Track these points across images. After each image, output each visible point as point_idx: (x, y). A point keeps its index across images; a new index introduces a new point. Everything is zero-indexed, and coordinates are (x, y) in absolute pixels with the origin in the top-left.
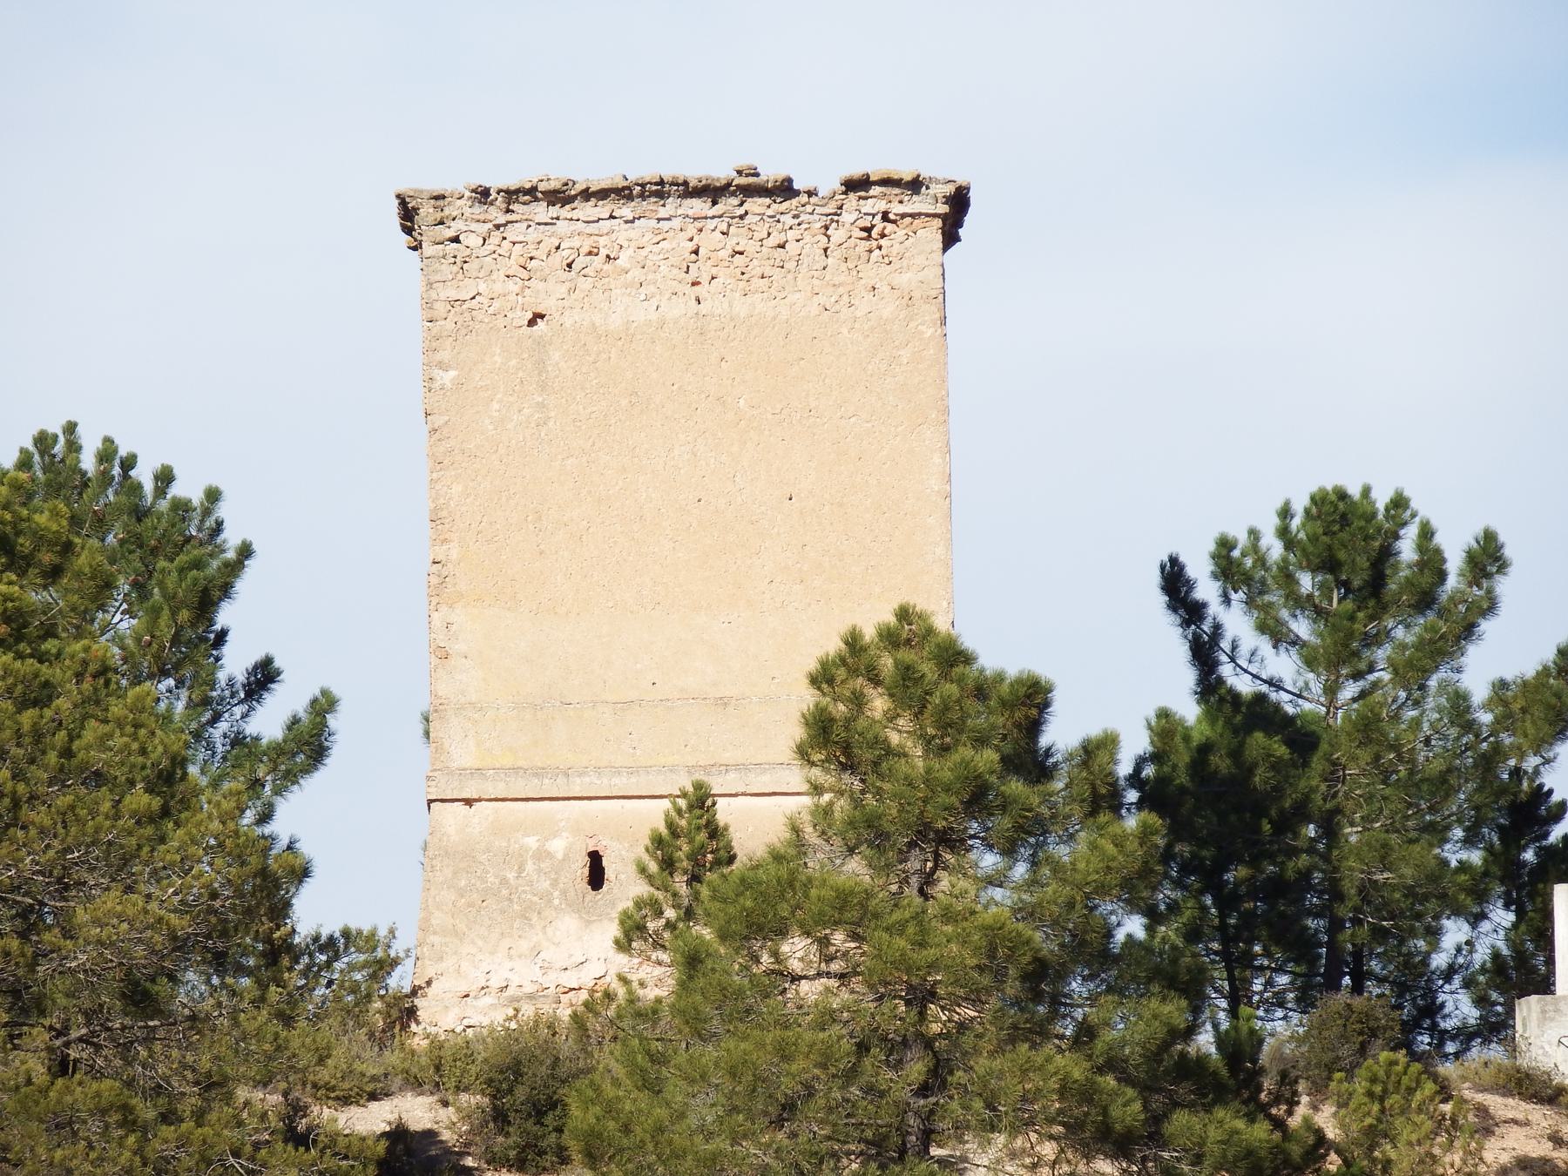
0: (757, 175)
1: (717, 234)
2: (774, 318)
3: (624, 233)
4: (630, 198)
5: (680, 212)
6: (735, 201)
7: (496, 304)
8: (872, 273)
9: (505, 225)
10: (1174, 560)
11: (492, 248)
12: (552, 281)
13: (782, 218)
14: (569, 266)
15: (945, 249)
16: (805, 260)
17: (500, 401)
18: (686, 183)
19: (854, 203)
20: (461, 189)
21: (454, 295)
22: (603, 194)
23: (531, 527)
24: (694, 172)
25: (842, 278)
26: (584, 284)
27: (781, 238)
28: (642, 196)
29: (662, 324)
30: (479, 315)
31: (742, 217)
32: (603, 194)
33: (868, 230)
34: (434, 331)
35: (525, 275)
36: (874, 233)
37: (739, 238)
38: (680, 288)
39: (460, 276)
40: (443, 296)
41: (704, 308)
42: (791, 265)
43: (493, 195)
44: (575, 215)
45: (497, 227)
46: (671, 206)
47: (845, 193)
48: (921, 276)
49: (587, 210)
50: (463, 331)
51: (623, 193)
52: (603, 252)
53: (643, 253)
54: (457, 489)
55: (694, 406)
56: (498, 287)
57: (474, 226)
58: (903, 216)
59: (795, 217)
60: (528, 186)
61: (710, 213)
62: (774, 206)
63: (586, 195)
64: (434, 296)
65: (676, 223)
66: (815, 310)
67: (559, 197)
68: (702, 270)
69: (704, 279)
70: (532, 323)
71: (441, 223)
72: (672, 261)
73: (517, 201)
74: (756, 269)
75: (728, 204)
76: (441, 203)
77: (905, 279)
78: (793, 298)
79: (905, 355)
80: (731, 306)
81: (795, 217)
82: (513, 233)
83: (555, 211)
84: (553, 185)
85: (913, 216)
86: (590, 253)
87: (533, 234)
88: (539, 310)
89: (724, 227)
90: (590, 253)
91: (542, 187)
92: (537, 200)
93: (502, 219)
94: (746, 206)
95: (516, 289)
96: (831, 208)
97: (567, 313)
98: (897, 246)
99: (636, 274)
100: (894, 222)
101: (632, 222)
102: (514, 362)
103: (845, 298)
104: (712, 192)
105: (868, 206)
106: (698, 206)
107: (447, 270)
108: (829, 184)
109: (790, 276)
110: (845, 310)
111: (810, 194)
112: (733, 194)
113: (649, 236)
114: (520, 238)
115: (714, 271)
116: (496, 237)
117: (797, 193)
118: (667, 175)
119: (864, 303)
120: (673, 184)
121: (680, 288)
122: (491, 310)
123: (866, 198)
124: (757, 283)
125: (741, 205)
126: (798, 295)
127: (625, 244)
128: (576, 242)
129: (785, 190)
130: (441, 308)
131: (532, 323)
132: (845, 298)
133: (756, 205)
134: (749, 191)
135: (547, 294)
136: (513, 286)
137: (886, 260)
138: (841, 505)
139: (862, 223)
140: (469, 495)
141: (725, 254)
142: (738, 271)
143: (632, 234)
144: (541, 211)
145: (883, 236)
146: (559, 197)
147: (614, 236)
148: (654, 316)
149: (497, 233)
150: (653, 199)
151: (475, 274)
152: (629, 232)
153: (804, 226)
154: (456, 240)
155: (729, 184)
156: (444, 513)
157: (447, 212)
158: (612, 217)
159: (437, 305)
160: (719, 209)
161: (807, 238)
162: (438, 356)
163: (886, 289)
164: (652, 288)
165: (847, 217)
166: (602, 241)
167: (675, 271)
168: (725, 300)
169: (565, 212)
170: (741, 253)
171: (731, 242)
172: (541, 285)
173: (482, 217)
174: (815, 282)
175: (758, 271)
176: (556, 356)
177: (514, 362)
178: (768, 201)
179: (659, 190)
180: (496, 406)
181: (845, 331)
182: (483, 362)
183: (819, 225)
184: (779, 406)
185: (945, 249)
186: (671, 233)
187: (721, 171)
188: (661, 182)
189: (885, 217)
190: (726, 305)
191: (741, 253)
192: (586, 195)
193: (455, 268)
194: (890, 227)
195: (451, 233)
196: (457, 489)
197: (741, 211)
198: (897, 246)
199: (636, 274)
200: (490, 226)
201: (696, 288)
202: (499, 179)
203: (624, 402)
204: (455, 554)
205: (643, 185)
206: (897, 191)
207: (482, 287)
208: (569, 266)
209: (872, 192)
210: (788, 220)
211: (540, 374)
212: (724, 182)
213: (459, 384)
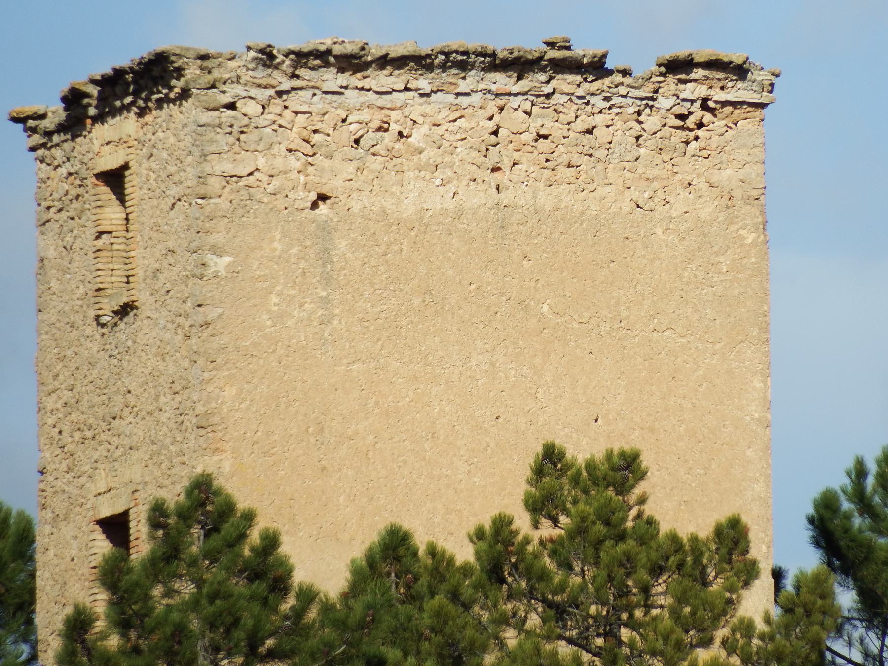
0: (568, 48)
1: (520, 114)
2: (583, 213)
3: (417, 107)
4: (430, 68)
5: (481, 86)
6: (543, 77)
7: (276, 182)
8: (688, 168)
9: (287, 92)
10: (735, 523)
11: (271, 117)
12: (338, 156)
13: (593, 100)
14: (357, 141)
15: (126, 167)
16: (617, 149)
17: (279, 295)
18: (494, 55)
19: (673, 87)
20: (240, 49)
21: (229, 168)
22: (400, 62)
23: (312, 440)
24: (502, 44)
25: (656, 172)
26: (375, 164)
27: (590, 122)
28: (444, 67)
29: (460, 213)
30: (258, 194)
31: (548, 96)
32: (400, 62)
33: (682, 117)
34: (208, 209)
35: (308, 150)
36: (691, 122)
37: (543, 120)
38: (480, 174)
39: (236, 148)
40: (218, 169)
41: (506, 197)
42: (601, 154)
43: (280, 58)
44: (366, 83)
45: (280, 94)
46: (471, 81)
47: (662, 75)
48: (742, 174)
49: (380, 79)
50: (240, 212)
51: (421, 62)
52: (394, 128)
53: (440, 130)
54: (230, 392)
55: (494, 309)
56: (279, 163)
57: (254, 92)
58: (724, 104)
59: (607, 99)
60: (322, 48)
61: (515, 89)
62: (586, 86)
63: (384, 62)
64: (208, 170)
65: (476, 99)
66: (627, 206)
67: (352, 63)
68: (503, 154)
69: (506, 164)
70: (314, 205)
71: (213, 87)
72: (470, 141)
73: (306, 66)
74: (562, 154)
75: (535, 80)
76: (207, 63)
77: (726, 176)
78: (601, 192)
79: (725, 261)
80: (535, 197)
81: (607, 99)
82: (295, 101)
83: (344, 79)
84: (350, 49)
85: (734, 104)
86: (380, 129)
87: (319, 103)
88: (324, 191)
89: (527, 106)
90: (380, 129)
91: (337, 50)
92: (327, 64)
93: (286, 85)
94: (554, 83)
95: (298, 165)
96: (645, 92)
97: (355, 195)
98: (716, 138)
99: (431, 154)
100: (712, 111)
101: (428, 95)
102: (295, 250)
103: (660, 194)
104: (520, 65)
105: (692, 91)
106: (502, 81)
107: (223, 141)
108: (645, 64)
109: (600, 166)
110: (659, 208)
111: (625, 73)
112: (543, 69)
113: (445, 112)
114: (304, 108)
115: (516, 156)
116: (276, 106)
117: (610, 73)
118: (473, 44)
119: (681, 200)
120: (483, 54)
121: (480, 174)
122: (270, 189)
123: (685, 82)
124: (564, 172)
125: (548, 82)
126: (608, 189)
127: (420, 120)
128: (365, 115)
129: (597, 68)
130: (215, 183)
131: (314, 205)
132: (660, 194)
133: (566, 82)
134: (562, 66)
135: (335, 173)
136: (295, 163)
137: (705, 153)
138: (652, 430)
139: (679, 110)
140: (244, 400)
141: (528, 137)
142: (542, 158)
143: (427, 109)
144: (331, 78)
145: (700, 125)
146: (352, 63)
147: (407, 111)
148: (450, 204)
149: (278, 101)
150: (454, 71)
151: (252, 147)
152: (427, 111)
153: (616, 110)
154: (232, 106)
155: (541, 58)
156: (215, 419)
157: (216, 74)
158: (407, 89)
159: (212, 180)
160: (524, 85)
161: (619, 124)
162: (213, 239)
163: (703, 186)
164: (449, 172)
165: (664, 102)
166: (395, 115)
167: (474, 154)
168: (527, 190)
169: (355, 80)
170: (545, 137)
171: (535, 125)
172: (327, 163)
173: (264, 82)
174: (628, 175)
175: (565, 159)
176: (342, 245)
177: (295, 250)
178: (579, 78)
179: (459, 61)
180: (275, 299)
181: (659, 231)
182: (261, 248)
183: (631, 110)
184: (586, 315)
185: (126, 167)
186: (470, 111)
187: (531, 44)
188: (465, 53)
189: (704, 106)
190: (529, 196)
191: (545, 137)
192: (384, 62)
193: (231, 139)
194: (708, 117)
195: (227, 99)
196: (230, 392)
197: (548, 89)
198: (716, 138)
199: (431, 154)
200: (271, 92)
201: (497, 174)
202: (286, 40)
203: (417, 302)
204: (227, 467)
205: (447, 54)
206: (721, 75)
207: (261, 162)
208: (357, 141)
209: (693, 76)
210: (598, 102)
211: (324, 266)
212: (537, 55)
213: (234, 272)
